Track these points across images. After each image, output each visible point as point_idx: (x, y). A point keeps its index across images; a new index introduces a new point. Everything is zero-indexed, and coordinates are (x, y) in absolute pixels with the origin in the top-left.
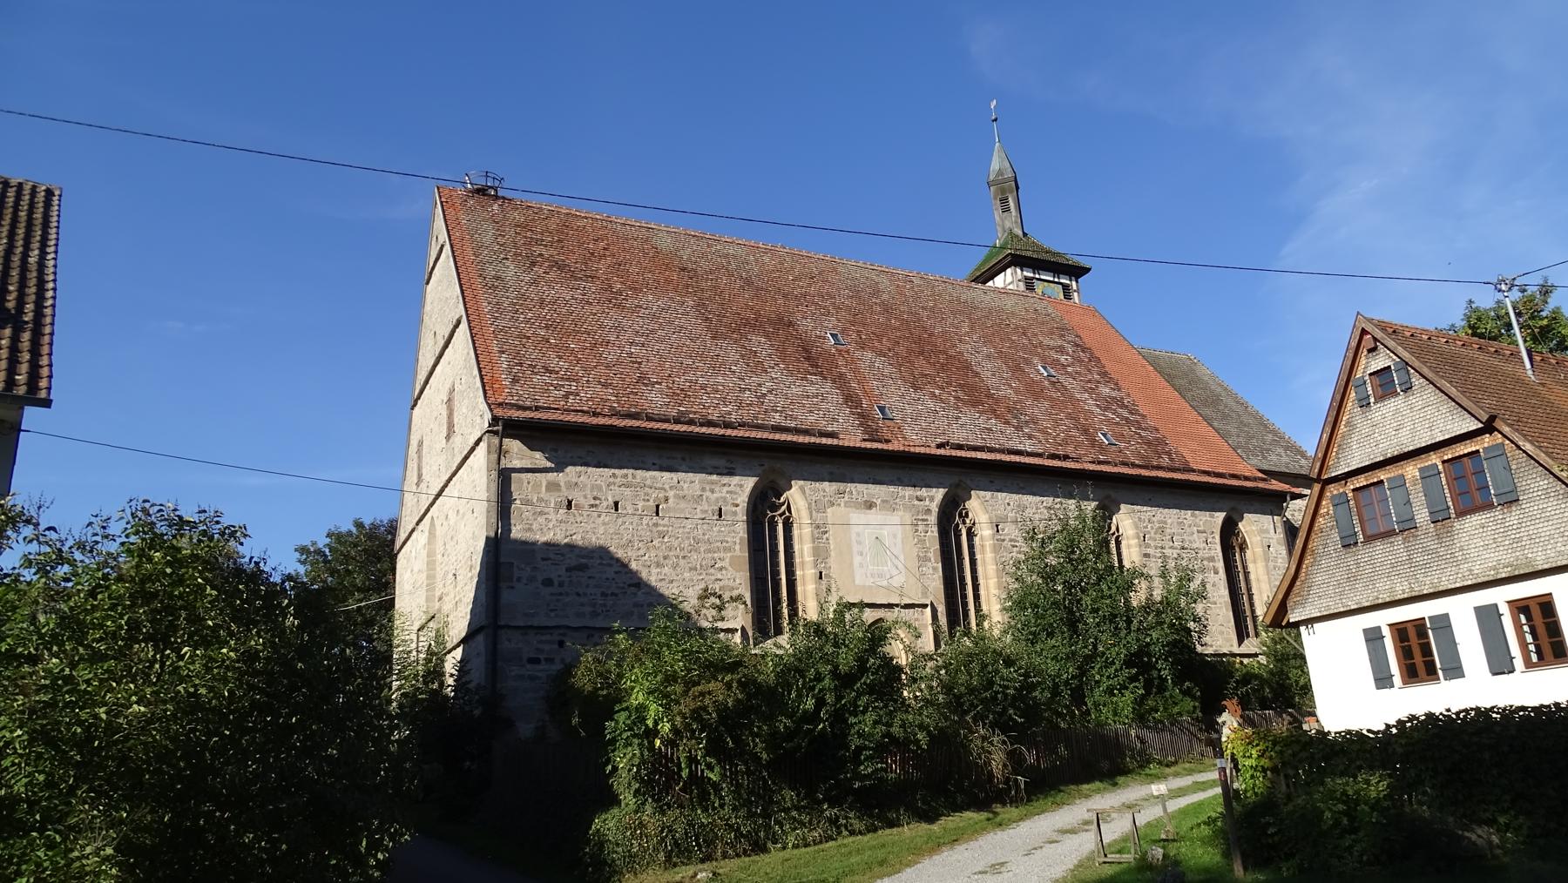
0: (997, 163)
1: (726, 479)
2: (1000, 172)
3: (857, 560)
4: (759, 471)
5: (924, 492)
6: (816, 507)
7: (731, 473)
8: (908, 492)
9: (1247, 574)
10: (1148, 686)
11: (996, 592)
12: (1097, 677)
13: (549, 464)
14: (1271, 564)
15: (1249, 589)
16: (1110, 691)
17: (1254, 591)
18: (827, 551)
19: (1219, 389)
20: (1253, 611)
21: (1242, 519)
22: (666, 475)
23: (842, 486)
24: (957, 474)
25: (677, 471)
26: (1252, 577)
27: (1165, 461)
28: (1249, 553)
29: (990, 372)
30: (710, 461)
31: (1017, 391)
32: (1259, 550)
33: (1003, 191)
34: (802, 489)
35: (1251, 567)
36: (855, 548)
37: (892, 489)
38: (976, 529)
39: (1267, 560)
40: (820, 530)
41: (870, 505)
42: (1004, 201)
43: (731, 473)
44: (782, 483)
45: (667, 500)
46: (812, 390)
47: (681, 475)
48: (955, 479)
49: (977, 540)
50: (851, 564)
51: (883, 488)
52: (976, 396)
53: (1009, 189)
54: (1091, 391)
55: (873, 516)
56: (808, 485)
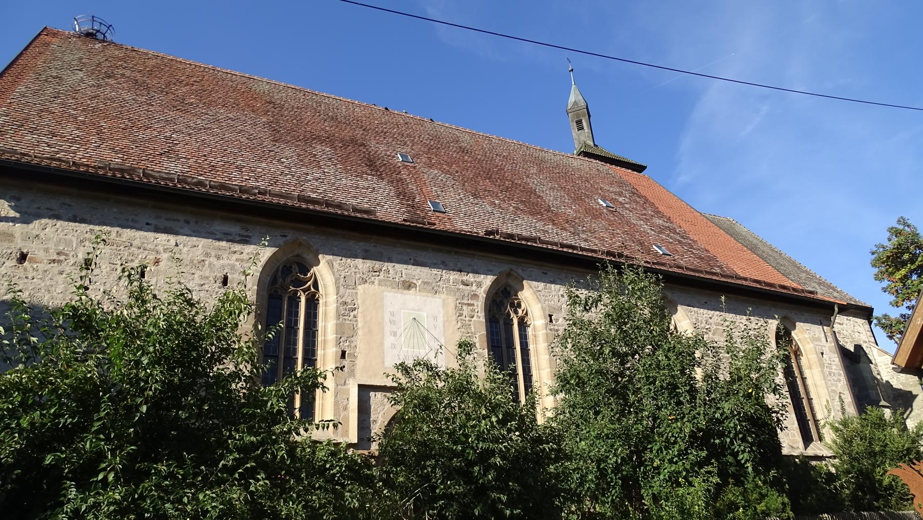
0: (574, 97)
1: (237, 247)
2: (575, 103)
3: (389, 340)
4: (281, 241)
5: (471, 277)
6: (343, 283)
7: (245, 241)
8: (454, 276)
9: (804, 379)
10: (722, 474)
11: (550, 382)
12: (657, 463)
13: (12, 214)
14: (826, 370)
15: (807, 393)
16: (673, 481)
17: (812, 395)
18: (354, 329)
19: (755, 241)
20: (814, 415)
21: (794, 328)
22: (162, 237)
23: (377, 265)
24: (510, 259)
25: (176, 233)
26: (809, 382)
27: (718, 270)
28: (804, 361)
29: (551, 197)
30: (218, 226)
31: (575, 211)
32: (814, 357)
33: (578, 115)
34: (331, 265)
35: (807, 373)
36: (388, 328)
37: (435, 271)
38: (529, 320)
39: (822, 366)
40: (347, 309)
41: (408, 286)
42: (579, 122)
43: (245, 240)
44: (309, 257)
45: (157, 262)
46: (362, 183)
47: (181, 239)
48: (506, 268)
49: (530, 331)
50: (382, 344)
51: (426, 270)
52: (533, 206)
53: (583, 117)
54: (646, 221)
55: (412, 298)
56: (337, 261)
